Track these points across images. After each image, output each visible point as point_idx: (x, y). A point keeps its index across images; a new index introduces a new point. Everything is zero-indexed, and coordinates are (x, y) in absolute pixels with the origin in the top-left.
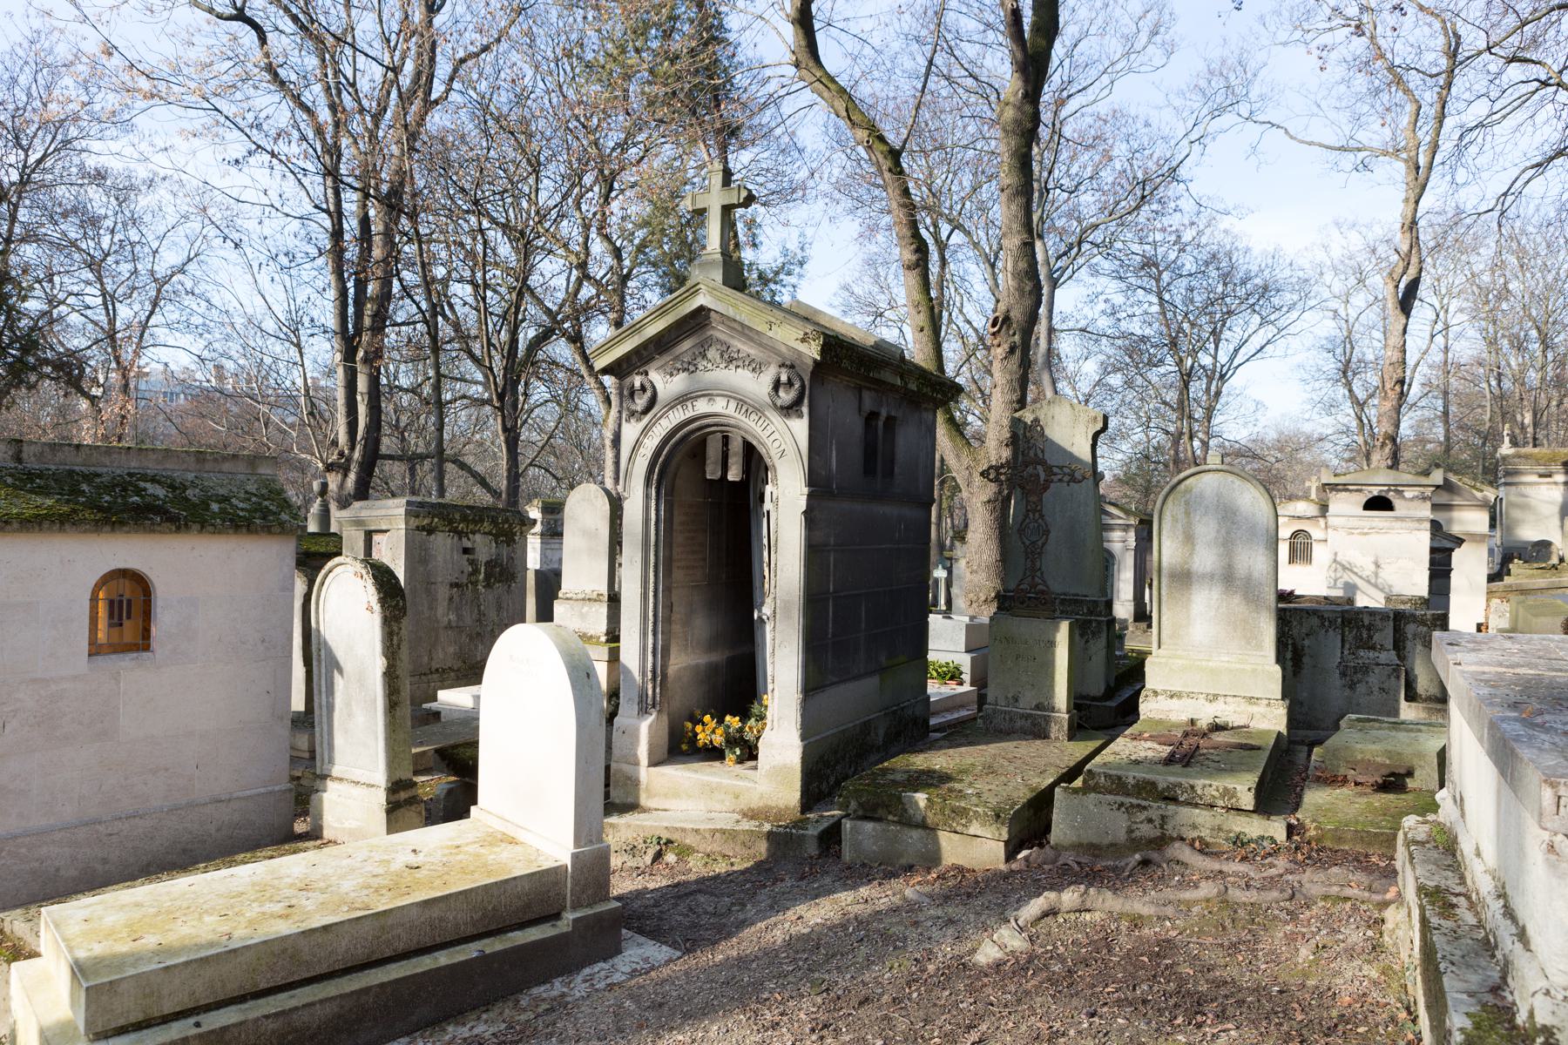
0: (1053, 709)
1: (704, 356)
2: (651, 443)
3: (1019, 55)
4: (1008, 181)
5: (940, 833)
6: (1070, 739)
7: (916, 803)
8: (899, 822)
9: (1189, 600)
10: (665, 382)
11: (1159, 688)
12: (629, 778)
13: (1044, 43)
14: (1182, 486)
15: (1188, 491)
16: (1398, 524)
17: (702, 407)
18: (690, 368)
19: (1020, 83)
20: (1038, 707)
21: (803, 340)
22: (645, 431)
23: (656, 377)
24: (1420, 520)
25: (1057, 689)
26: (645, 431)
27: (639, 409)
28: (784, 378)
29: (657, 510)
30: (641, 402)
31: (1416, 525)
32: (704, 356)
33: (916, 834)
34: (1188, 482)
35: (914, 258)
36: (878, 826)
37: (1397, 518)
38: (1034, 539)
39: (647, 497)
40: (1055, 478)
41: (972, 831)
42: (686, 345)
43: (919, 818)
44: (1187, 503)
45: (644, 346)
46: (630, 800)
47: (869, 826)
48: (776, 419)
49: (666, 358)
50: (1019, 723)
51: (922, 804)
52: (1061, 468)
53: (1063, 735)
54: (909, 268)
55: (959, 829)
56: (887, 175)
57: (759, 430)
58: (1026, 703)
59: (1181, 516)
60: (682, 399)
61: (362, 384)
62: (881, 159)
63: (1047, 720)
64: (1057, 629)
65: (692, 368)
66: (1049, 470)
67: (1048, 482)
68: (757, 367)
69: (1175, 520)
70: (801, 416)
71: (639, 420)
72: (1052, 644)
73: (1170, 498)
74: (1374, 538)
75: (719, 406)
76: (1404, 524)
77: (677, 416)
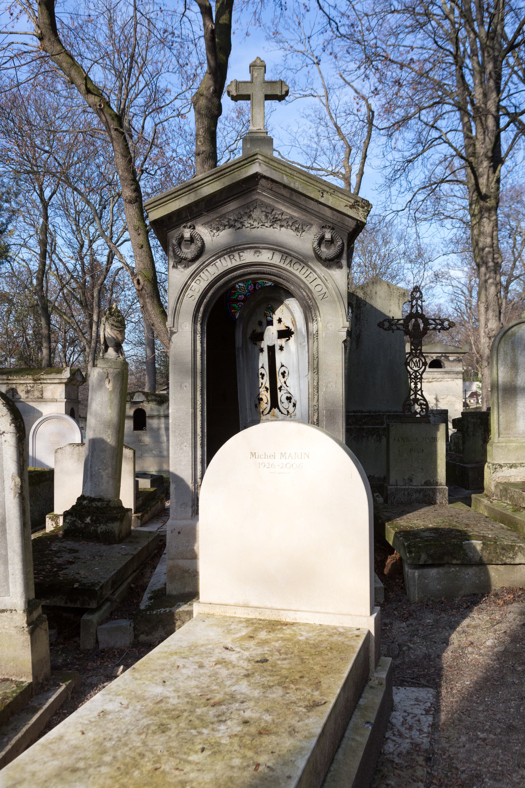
0: (436, 484)
1: (250, 216)
2: (198, 287)
3: (212, 63)
4: (203, 148)
5: (490, 567)
6: (450, 502)
7: (474, 548)
8: (462, 565)
9: (516, 405)
10: (209, 235)
11: (502, 462)
12: (187, 571)
13: (224, 58)
14: (510, 332)
15: (514, 335)
16: (446, 376)
17: (248, 257)
18: (235, 224)
19: (211, 82)
20: (427, 483)
21: (352, 207)
22: (193, 276)
23: (203, 232)
24: (457, 373)
25: (439, 470)
26: (193, 276)
27: (189, 256)
28: (328, 236)
29: (202, 343)
30: (188, 252)
31: (456, 376)
32: (250, 216)
33: (471, 571)
34: (513, 329)
35: (134, 195)
36: (441, 570)
37: (447, 372)
38: (416, 369)
39: (195, 332)
40: (431, 327)
41: (517, 561)
42: (232, 206)
43: (477, 559)
44: (513, 343)
45: (196, 204)
46: (188, 590)
47: (433, 572)
48: (320, 269)
49: (213, 215)
50: (415, 496)
51: (479, 548)
52: (434, 320)
53: (445, 501)
54: (130, 202)
55: (508, 561)
56: (113, 133)
57: (303, 277)
58: (418, 482)
59: (509, 351)
60: (229, 250)
61: (242, 163)
62: (109, 120)
63: (434, 491)
64: (437, 429)
65: (238, 225)
66: (426, 321)
67: (426, 329)
68: (299, 227)
69: (506, 354)
70: (341, 267)
71: (186, 266)
72: (434, 440)
73: (502, 342)
74: (434, 384)
75: (265, 257)
76: (450, 376)
77: (225, 264)
